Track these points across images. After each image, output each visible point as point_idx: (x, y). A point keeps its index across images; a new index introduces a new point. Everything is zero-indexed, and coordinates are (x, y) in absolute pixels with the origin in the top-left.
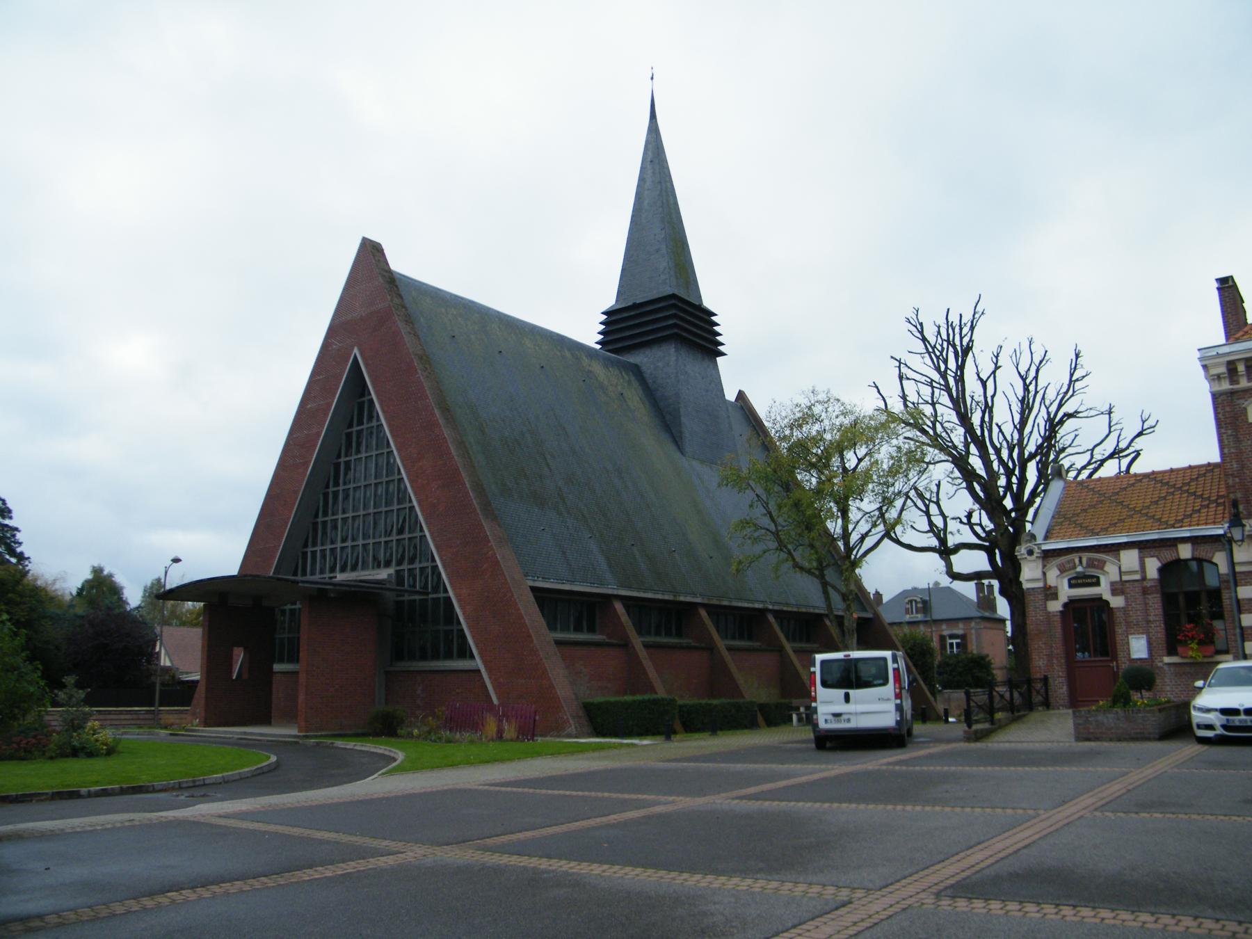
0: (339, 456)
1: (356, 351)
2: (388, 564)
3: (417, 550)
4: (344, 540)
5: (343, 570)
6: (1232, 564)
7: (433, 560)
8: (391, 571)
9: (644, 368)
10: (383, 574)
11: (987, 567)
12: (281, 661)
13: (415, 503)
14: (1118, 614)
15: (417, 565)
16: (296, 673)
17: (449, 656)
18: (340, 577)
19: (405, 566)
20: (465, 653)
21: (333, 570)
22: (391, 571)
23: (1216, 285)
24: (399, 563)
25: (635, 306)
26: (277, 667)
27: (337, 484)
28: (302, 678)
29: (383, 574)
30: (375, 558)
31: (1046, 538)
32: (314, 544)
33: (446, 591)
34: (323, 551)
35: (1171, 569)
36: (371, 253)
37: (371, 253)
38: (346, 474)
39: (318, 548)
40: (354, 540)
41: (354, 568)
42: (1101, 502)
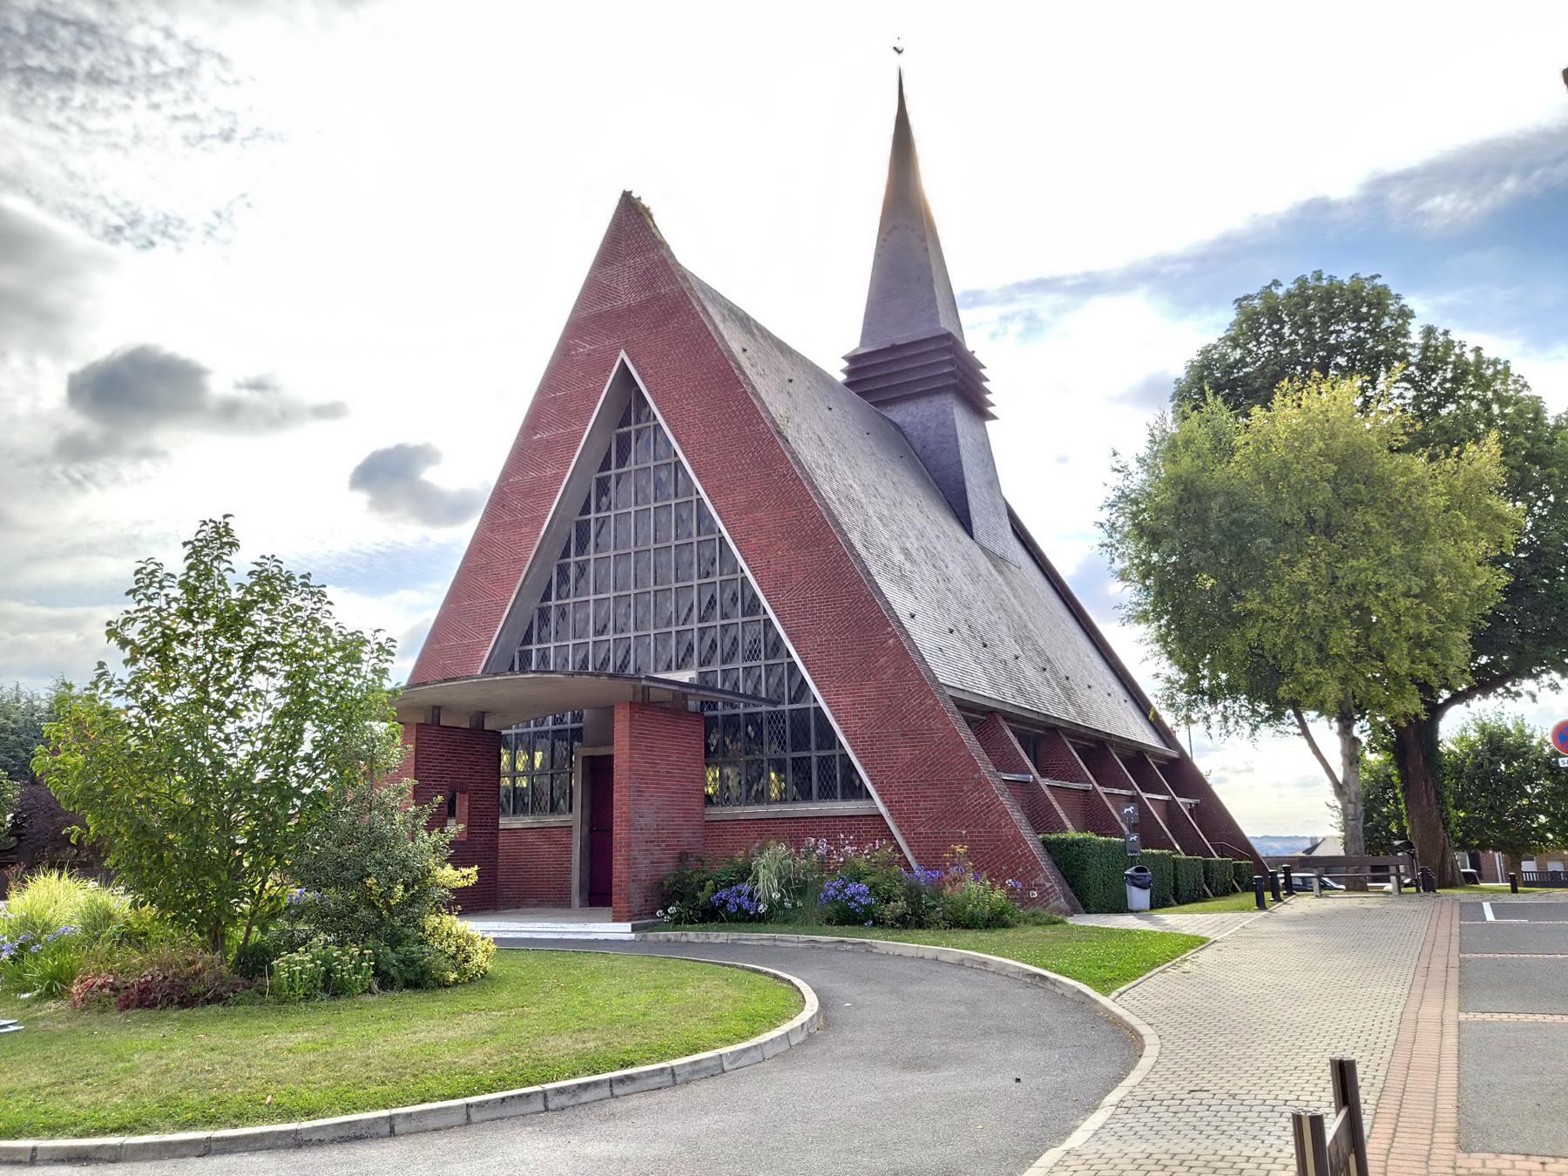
1: (623, 354)
9: (907, 430)
13: (748, 573)
14: (1062, 903)
17: (827, 794)
20: (855, 790)
25: (895, 348)
26: (504, 822)
29: (685, 676)
36: (632, 224)
37: (632, 224)
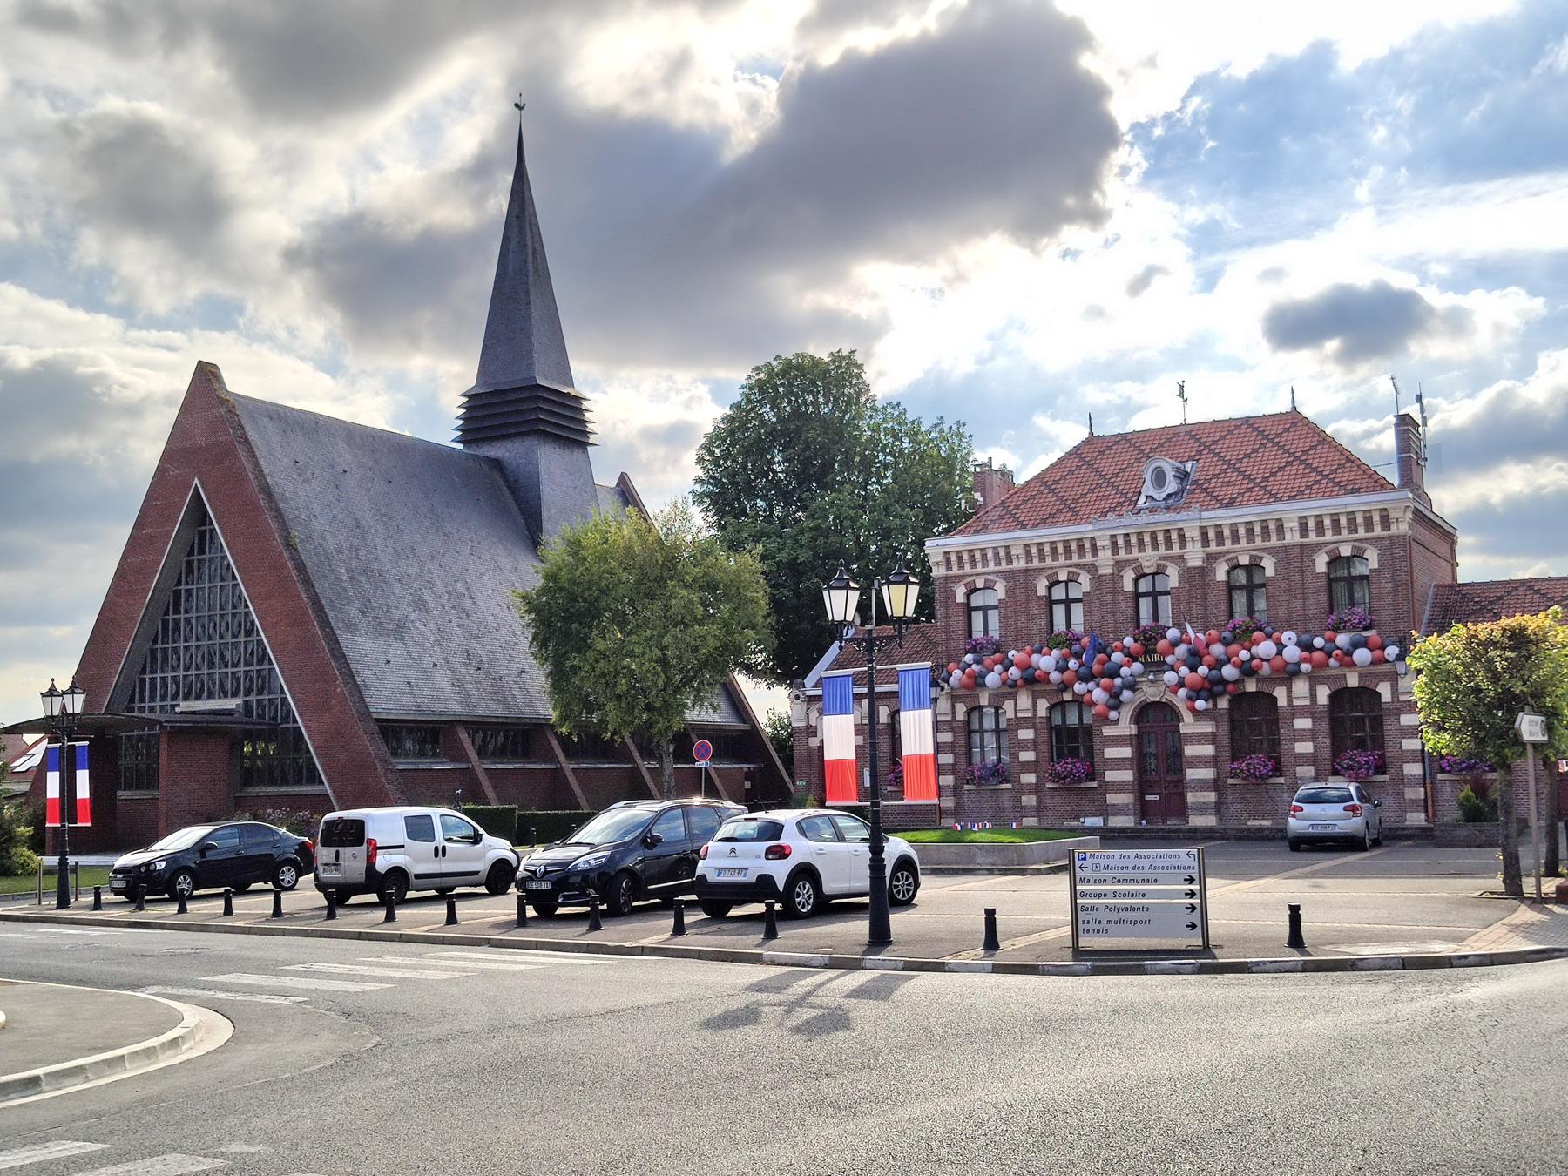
0: (179, 583)
1: (196, 481)
2: (235, 695)
3: (264, 682)
4: (187, 668)
5: (186, 698)
6: (1290, 698)
7: (282, 692)
8: (239, 701)
10: (232, 704)
11: (271, 897)
12: (127, 787)
15: (266, 697)
16: (155, 799)
18: (184, 706)
19: (253, 697)
20: (314, 779)
21: (174, 698)
22: (239, 701)
23: (1292, 46)
24: (247, 693)
26: (119, 793)
27: (177, 611)
28: (162, 806)
29: (232, 704)
30: (222, 686)
31: (815, 686)
32: (153, 671)
33: (295, 721)
34: (153, 680)
35: (1339, 696)
38: (187, 600)
39: (158, 676)
40: (198, 668)
41: (198, 697)
42: (1279, 435)
